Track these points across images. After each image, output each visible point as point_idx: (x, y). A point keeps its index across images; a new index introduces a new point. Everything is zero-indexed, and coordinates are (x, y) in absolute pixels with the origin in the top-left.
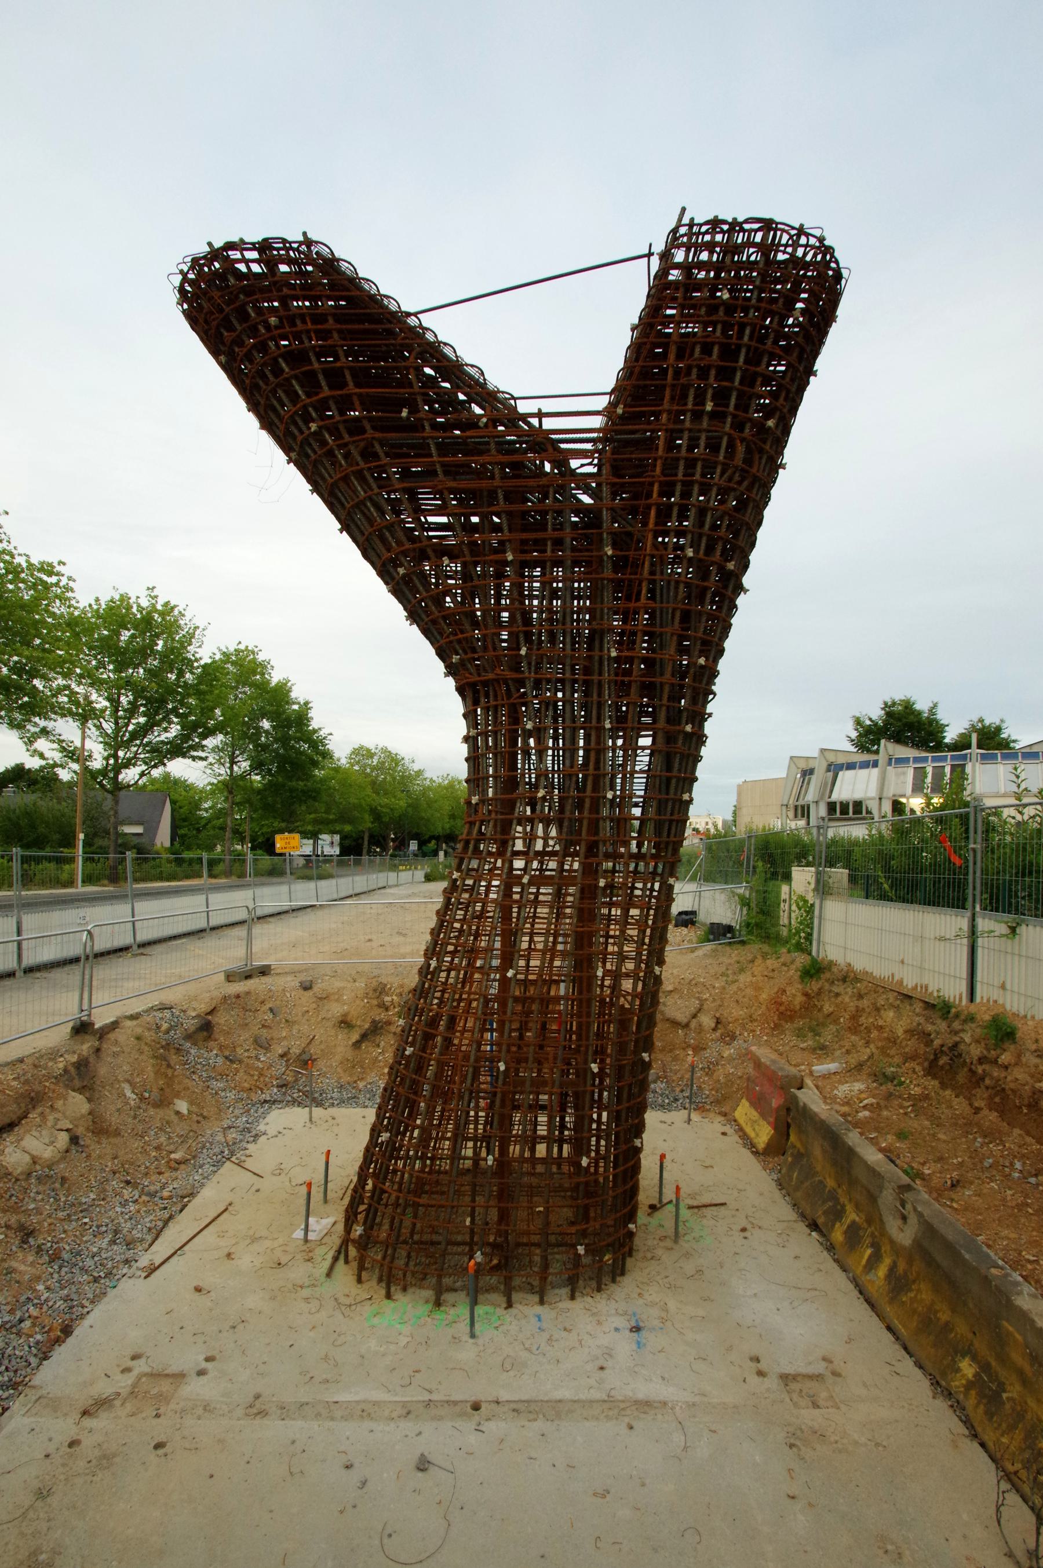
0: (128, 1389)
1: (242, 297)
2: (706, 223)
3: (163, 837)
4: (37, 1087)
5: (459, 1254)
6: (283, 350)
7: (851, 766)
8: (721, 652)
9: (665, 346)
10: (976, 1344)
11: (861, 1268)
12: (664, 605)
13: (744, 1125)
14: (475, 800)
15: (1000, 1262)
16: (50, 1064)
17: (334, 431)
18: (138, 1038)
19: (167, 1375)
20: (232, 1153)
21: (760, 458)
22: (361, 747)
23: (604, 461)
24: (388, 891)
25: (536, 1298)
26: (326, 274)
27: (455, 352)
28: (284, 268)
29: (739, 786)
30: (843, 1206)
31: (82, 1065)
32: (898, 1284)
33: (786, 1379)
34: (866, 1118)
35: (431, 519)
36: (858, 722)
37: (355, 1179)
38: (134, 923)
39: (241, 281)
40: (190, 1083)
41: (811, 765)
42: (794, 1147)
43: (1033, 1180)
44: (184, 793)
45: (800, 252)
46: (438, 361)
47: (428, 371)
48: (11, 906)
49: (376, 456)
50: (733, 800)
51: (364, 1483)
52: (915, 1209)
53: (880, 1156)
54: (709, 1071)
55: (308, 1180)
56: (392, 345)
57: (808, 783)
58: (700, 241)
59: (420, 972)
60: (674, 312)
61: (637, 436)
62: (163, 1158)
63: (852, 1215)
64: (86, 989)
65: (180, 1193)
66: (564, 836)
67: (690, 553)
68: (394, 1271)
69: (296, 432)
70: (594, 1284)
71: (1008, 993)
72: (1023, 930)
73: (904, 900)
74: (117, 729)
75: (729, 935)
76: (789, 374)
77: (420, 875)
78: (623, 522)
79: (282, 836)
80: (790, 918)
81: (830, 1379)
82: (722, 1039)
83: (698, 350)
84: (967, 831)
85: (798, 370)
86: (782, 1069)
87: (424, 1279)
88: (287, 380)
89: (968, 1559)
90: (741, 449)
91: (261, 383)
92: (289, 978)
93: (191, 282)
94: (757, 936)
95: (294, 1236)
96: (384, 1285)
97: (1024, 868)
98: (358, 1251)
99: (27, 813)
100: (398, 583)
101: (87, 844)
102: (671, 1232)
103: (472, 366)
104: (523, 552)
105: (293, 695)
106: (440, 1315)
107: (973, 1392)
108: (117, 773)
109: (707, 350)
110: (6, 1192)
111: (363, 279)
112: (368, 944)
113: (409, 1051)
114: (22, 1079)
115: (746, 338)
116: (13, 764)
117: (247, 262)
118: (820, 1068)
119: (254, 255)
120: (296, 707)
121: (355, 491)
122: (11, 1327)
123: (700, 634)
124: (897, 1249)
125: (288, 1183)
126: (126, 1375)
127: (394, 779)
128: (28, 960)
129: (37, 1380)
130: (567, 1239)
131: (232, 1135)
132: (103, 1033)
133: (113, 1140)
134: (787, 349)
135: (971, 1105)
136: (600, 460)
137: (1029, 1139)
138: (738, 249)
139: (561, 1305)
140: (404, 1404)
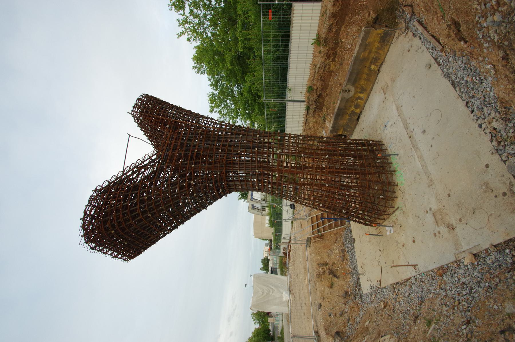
2: (133, 108)
11: (363, 101)
19: (435, 219)
29: (255, 238)
32: (363, 90)
33: (385, 94)
36: (240, 199)
41: (251, 206)
73: (285, 123)
81: (383, 88)
97: (277, 95)
135: (326, 96)
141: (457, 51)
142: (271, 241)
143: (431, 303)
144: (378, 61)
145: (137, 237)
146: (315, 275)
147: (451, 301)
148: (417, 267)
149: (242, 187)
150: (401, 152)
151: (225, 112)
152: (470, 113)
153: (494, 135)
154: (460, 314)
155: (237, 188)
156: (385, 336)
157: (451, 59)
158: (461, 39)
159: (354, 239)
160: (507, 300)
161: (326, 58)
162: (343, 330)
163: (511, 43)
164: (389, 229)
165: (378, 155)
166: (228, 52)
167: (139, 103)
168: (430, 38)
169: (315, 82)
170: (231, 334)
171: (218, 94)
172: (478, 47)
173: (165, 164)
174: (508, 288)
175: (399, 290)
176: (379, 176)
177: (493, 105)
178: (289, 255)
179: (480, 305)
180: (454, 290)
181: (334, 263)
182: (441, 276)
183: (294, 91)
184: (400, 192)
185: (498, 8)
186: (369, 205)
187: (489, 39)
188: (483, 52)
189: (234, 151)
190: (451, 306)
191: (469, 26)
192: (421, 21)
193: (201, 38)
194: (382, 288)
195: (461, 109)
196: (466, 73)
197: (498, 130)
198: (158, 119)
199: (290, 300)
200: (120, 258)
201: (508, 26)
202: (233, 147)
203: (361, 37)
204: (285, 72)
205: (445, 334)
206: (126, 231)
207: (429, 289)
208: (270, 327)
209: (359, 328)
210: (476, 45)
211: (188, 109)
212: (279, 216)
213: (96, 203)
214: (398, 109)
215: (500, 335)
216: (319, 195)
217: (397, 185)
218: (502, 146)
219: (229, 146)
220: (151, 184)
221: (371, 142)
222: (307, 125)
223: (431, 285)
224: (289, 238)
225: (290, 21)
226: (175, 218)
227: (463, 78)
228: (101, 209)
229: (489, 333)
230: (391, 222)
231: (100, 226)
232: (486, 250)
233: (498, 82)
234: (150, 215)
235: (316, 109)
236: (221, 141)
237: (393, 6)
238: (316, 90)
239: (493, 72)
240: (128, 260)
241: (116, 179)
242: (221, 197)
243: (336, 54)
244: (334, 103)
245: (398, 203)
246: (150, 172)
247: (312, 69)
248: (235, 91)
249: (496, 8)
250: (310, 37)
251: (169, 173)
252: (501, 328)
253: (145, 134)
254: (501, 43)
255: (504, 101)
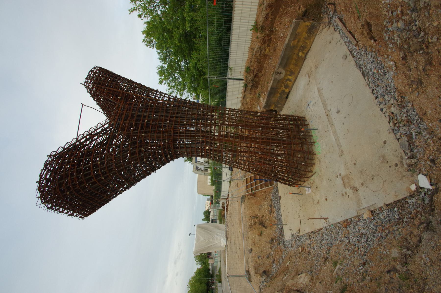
19: (343, 182)
29: (198, 194)
32: (292, 73)
33: (309, 77)
41: (195, 167)
73: (226, 98)
77: (219, 284)
124: (286, 75)
141: (368, 46)
142: (212, 196)
143: (338, 248)
144: (305, 49)
145: (91, 197)
146: (248, 226)
147: (353, 247)
148: (328, 219)
149: (187, 154)
150: (320, 127)
151: (174, 84)
152: (375, 99)
153: (391, 118)
154: (358, 257)
155: (183, 154)
156: (301, 274)
157: (363, 53)
158: (372, 38)
159: (280, 197)
160: (393, 247)
161: (263, 43)
163: (410, 47)
164: (308, 190)
165: (302, 129)
166: (176, 29)
167: (92, 75)
168: (347, 34)
169: (252, 63)
170: (177, 274)
171: (166, 67)
172: (384, 46)
173: (118, 132)
174: (394, 238)
175: (313, 237)
176: (302, 146)
177: (393, 94)
178: (227, 209)
179: (374, 250)
180: (355, 239)
181: (264, 216)
182: (346, 227)
184: (317, 160)
185: (402, 16)
186: (293, 170)
187: (393, 41)
188: (388, 51)
189: (181, 122)
190: (353, 251)
191: (379, 28)
192: (341, 18)
193: (151, 15)
194: (301, 236)
195: (368, 95)
196: (373, 65)
197: (395, 114)
198: (110, 90)
199: (227, 245)
200: (76, 216)
201: (408, 33)
202: (179, 119)
203: (292, 27)
205: (346, 273)
206: (80, 193)
207: (336, 237)
208: (210, 267)
209: (282, 267)
210: (383, 44)
211: (138, 83)
212: (219, 176)
213: (51, 167)
214: (319, 91)
215: (386, 274)
216: (253, 161)
217: (316, 154)
218: (397, 127)
219: (177, 117)
220: (104, 150)
221: (296, 118)
222: (244, 100)
223: (338, 234)
224: (227, 195)
225: (232, 8)
226: (127, 180)
227: (371, 70)
228: (56, 173)
229: (379, 272)
230: (309, 183)
231: (55, 188)
232: (381, 208)
233: (397, 76)
234: (103, 178)
235: (253, 87)
236: (169, 113)
237: (320, 3)
238: (253, 71)
239: (394, 68)
240: (83, 218)
241: (70, 146)
242: (169, 162)
243: (271, 41)
244: (268, 83)
245: (316, 168)
246: (103, 139)
247: (250, 52)
248: (183, 66)
249: (400, 16)
250: (249, 24)
251: (121, 140)
252: (387, 269)
253: (98, 104)
254: (402, 46)
255: (401, 92)
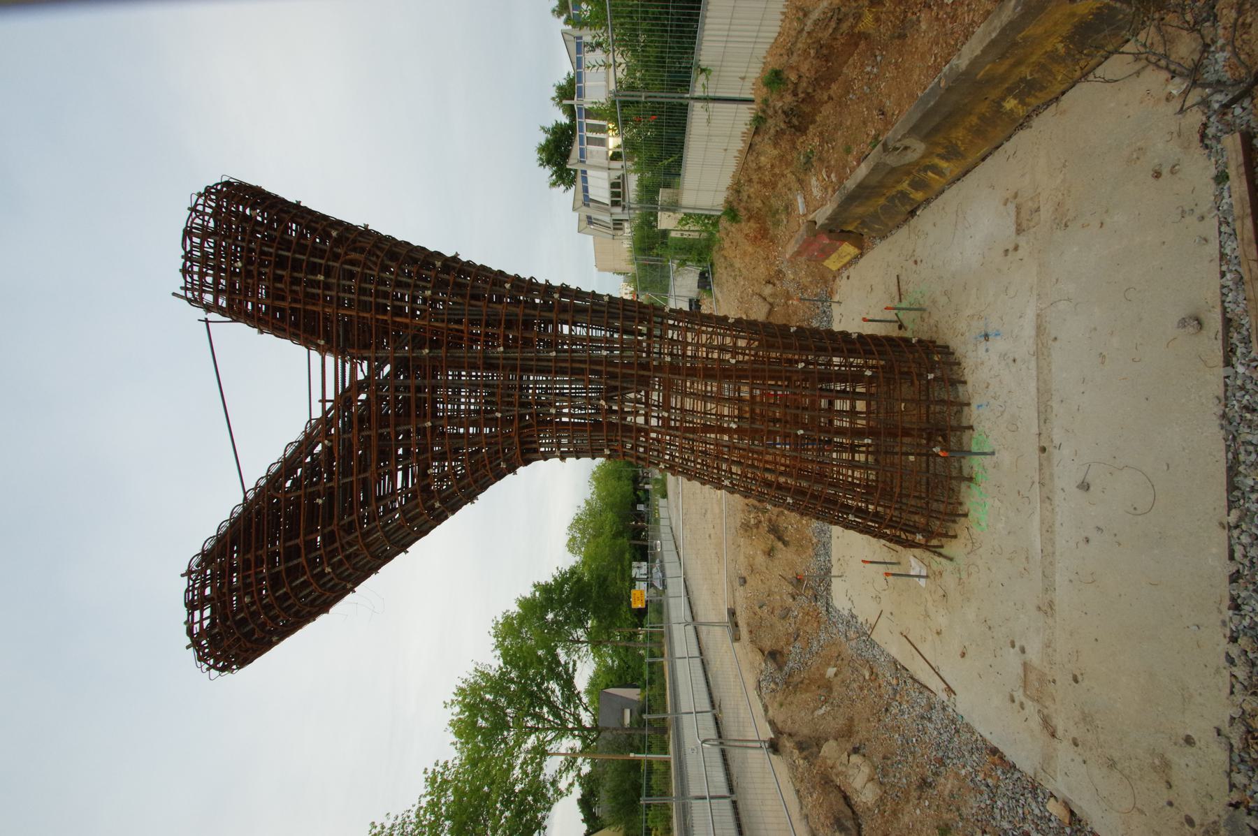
0: (1035, 704)
1: (228, 623)
2: (185, 278)
3: (633, 694)
4: (817, 779)
5: (935, 464)
6: (269, 592)
7: (586, 190)
8: (501, 273)
9: (276, 309)
10: (992, 97)
11: (941, 180)
12: (466, 312)
13: (842, 264)
14: (607, 452)
15: (936, 80)
16: (800, 770)
17: (332, 554)
18: (781, 705)
19: (1025, 676)
20: (865, 634)
21: (360, 242)
22: (568, 545)
23: (359, 355)
24: (674, 526)
25: (966, 409)
26: (213, 560)
27: (274, 464)
28: (208, 591)
30: (899, 192)
31: (801, 746)
32: (952, 153)
33: (1019, 230)
34: (836, 176)
35: (399, 486)
36: (554, 184)
37: (883, 542)
38: (697, 713)
39: (216, 624)
40: (815, 666)
41: (584, 218)
42: (856, 228)
43: (879, 58)
44: (600, 679)
45: (209, 210)
46: (280, 476)
47: (288, 484)
48: (684, 805)
49: (351, 523)
50: (609, 275)
51: (1099, 529)
52: (900, 140)
53: (863, 165)
54: (804, 289)
55: (882, 578)
56: (268, 511)
57: (598, 220)
58: (197, 283)
59: (732, 493)
60: (250, 304)
61: (341, 333)
62: (869, 685)
63: (905, 186)
64: (745, 744)
65: (894, 671)
66: (634, 386)
67: (428, 293)
68: (948, 511)
69: (331, 584)
70: (955, 368)
71: (748, 75)
72: (703, 64)
74: (552, 728)
75: (707, 275)
76: (300, 220)
77: (662, 502)
78: (405, 341)
79: (633, 603)
80: (693, 231)
81: (1019, 200)
82: (780, 280)
83: (279, 285)
84: (632, 103)
85: (295, 214)
86: (802, 236)
87: (953, 490)
88: (292, 589)
89: (1141, 102)
90: (353, 256)
91: (294, 610)
92: (737, 594)
93: (217, 662)
94: (707, 255)
95: (924, 586)
96: (957, 519)
97: (659, 62)
98: (934, 538)
99: (614, 797)
100: (447, 508)
101: (638, 751)
102: (918, 313)
103: (286, 451)
104: (425, 416)
105: (529, 596)
106: (979, 478)
107: (1027, 100)
108: (585, 728)
109: (279, 279)
110: (894, 800)
111: (218, 531)
112: (712, 536)
113: (790, 500)
114: (812, 790)
115: (271, 250)
116: (578, 807)
117: (202, 619)
118: (801, 208)
119: (197, 614)
120: (537, 594)
121: (377, 539)
122: (992, 793)
123: (488, 287)
125: (886, 592)
126: (1025, 706)
127: (592, 521)
128: (724, 791)
129: (1031, 773)
130: (923, 388)
131: (852, 634)
132: (778, 731)
133: (856, 723)
134: (280, 221)
135: (826, 102)
136: (358, 358)
137: (851, 61)
138: (205, 255)
139: (970, 391)
140: (1042, 501)
162: (782, 648)
183: (717, 74)
204: (690, 37)
